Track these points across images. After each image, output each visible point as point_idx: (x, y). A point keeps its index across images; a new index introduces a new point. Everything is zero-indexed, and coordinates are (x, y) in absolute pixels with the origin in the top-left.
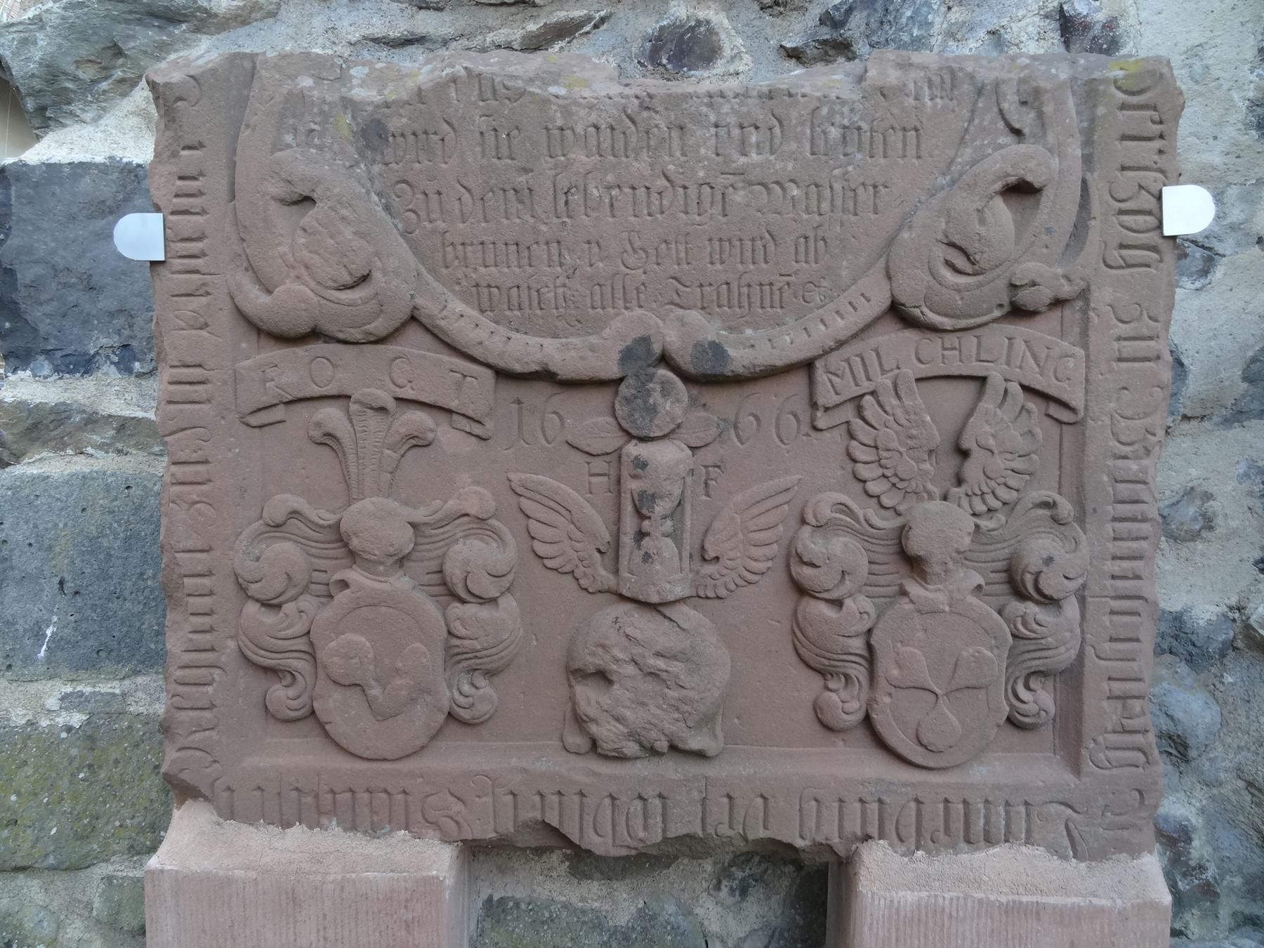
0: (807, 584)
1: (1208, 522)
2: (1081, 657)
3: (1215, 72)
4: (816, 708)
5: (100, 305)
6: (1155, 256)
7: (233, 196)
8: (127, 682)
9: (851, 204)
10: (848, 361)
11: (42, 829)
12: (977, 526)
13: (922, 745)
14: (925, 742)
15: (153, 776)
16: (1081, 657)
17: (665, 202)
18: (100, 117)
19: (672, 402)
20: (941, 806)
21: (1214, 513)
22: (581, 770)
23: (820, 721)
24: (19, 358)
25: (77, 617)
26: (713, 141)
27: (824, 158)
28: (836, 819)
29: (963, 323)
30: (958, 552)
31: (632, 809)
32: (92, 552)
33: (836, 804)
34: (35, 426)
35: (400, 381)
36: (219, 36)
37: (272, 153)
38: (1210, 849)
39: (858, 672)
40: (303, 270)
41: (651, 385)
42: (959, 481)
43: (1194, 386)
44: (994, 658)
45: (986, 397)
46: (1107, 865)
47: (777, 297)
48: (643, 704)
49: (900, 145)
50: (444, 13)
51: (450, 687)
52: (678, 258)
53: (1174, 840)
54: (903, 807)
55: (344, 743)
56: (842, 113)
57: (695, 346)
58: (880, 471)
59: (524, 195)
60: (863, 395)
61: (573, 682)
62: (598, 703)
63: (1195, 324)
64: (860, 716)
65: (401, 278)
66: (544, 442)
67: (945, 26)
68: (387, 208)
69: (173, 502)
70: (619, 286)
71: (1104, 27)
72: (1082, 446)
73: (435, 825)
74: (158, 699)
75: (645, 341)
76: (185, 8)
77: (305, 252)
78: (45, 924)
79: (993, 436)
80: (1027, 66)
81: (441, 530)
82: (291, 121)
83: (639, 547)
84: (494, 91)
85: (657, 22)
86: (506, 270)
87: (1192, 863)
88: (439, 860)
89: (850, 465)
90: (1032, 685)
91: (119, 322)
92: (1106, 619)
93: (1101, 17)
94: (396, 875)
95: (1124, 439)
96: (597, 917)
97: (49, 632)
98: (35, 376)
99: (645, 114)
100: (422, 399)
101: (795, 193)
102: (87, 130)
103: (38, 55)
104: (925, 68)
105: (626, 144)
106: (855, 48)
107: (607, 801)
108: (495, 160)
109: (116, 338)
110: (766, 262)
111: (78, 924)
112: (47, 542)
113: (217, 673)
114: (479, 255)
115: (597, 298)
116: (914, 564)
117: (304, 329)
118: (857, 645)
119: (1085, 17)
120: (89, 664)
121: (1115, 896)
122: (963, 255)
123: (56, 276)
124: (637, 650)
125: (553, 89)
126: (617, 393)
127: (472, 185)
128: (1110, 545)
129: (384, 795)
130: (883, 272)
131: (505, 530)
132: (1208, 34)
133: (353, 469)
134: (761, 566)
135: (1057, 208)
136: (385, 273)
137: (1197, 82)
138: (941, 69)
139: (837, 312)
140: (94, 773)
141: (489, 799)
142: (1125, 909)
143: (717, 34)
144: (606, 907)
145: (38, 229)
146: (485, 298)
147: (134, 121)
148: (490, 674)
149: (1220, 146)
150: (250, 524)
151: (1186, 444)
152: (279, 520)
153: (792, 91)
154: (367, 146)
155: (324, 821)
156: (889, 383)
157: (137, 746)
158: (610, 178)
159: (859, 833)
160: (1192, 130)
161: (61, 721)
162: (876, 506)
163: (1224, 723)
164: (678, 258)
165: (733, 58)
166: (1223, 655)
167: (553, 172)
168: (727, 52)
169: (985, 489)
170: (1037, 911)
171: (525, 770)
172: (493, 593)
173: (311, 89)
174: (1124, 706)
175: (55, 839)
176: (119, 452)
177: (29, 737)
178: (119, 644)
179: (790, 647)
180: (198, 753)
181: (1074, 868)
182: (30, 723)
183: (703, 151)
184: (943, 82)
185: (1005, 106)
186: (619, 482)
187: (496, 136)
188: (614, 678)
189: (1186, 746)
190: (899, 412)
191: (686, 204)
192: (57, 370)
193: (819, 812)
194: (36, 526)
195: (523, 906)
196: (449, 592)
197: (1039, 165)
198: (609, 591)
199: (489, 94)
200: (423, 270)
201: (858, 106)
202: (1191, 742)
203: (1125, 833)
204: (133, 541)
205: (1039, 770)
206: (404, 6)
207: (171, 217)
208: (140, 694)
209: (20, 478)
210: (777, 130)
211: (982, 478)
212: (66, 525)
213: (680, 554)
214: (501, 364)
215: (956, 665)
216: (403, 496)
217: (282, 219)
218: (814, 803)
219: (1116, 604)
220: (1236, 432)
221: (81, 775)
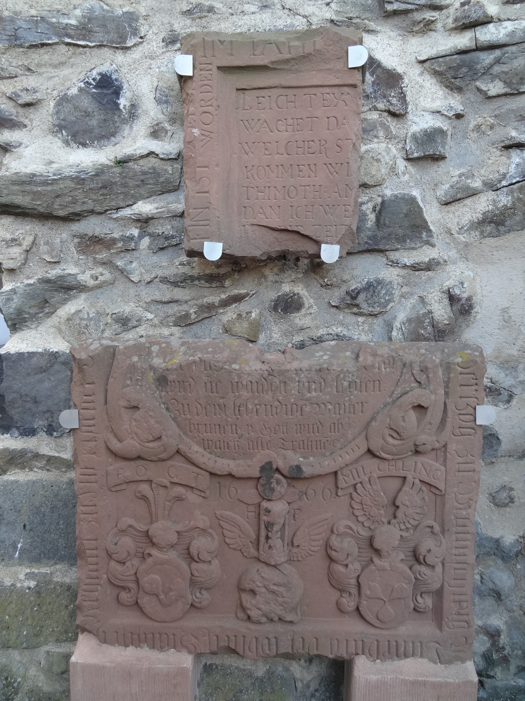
0: (334, 558)
1: (512, 500)
2: (442, 586)
3: (513, 319)
4: (337, 604)
5: (40, 409)
6: (474, 431)
7: (106, 403)
8: (52, 568)
9: (352, 410)
10: (351, 471)
11: (20, 631)
12: (401, 536)
13: (378, 619)
14: (380, 619)
15: (66, 610)
16: (442, 586)
17: (278, 411)
18: (38, 326)
19: (281, 487)
20: (387, 643)
21: (514, 496)
22: (243, 627)
23: (339, 609)
24: (6, 429)
25: (32, 540)
26: (297, 388)
27: (341, 394)
28: (345, 647)
29: (396, 457)
30: (393, 547)
31: (264, 642)
32: (37, 513)
33: (345, 642)
34: (12, 458)
35: (172, 476)
36: (89, 294)
37: (122, 389)
38: (508, 639)
39: (354, 591)
40: (134, 435)
41: (272, 480)
42: (395, 517)
44: (408, 588)
45: (405, 485)
46: (452, 666)
47: (322, 445)
48: (269, 603)
49: (372, 387)
50: (186, 289)
51: (192, 594)
52: (283, 432)
54: (371, 643)
55: (150, 615)
56: (349, 377)
57: (290, 467)
58: (363, 513)
59: (223, 407)
60: (357, 484)
61: (240, 592)
62: (250, 602)
63: (504, 423)
64: (355, 607)
65: (173, 436)
66: (229, 499)
67: (400, 293)
68: (167, 409)
69: (82, 521)
70: (259, 442)
71: (466, 300)
72: (443, 504)
73: (186, 647)
74: (66, 575)
75: (270, 463)
76: (75, 285)
77: (135, 429)
78: (21, 669)
79: (409, 501)
80: (423, 355)
81: (188, 533)
82: (129, 375)
83: (267, 542)
84: (210, 367)
85: (277, 294)
86: (215, 434)
87: (500, 646)
88: (186, 660)
89: (351, 510)
90: (423, 596)
91: (48, 415)
92: (452, 572)
93: (465, 295)
94: (170, 666)
95: (460, 502)
96: (250, 672)
97: (19, 546)
98: (11, 437)
99: (270, 377)
100: (180, 483)
101: (330, 407)
102: (34, 332)
103: (14, 306)
104: (382, 356)
105: (263, 388)
106: (361, 305)
107: (254, 639)
108: (210, 393)
109: (46, 422)
110: (318, 433)
111: (34, 668)
112: (18, 509)
113: (99, 587)
114: (204, 428)
115: (251, 446)
117: (135, 456)
118: (353, 581)
119: (459, 295)
120: (36, 560)
121: (454, 678)
122: (397, 433)
123: (21, 397)
124: (266, 583)
125: (234, 366)
126: (258, 482)
127: (201, 402)
128: (454, 543)
129: (166, 636)
130: (365, 437)
131: (214, 534)
132: (511, 303)
133: (153, 509)
134: (316, 549)
135: (434, 415)
136: (167, 436)
137: (506, 322)
138: (389, 357)
139: (347, 452)
140: (40, 608)
141: (207, 638)
142: (459, 683)
143: (302, 298)
144: (253, 668)
145: (14, 379)
147: (53, 330)
148: (207, 589)
149: (516, 347)
150: (112, 529)
151: (503, 466)
152: (124, 529)
153: (329, 368)
154: (159, 385)
155: (142, 645)
156: (367, 479)
157: (58, 596)
158: (256, 401)
159: (354, 652)
160: (505, 340)
161: (26, 584)
162: (362, 526)
163: (516, 585)
164: (283, 432)
165: (309, 308)
166: (517, 556)
167: (234, 399)
168: (306, 305)
169: (405, 520)
170: (424, 684)
171: (222, 627)
172: (209, 559)
173: (137, 362)
174: (460, 604)
175: (26, 636)
176: (48, 470)
177: (13, 591)
178: (49, 551)
179: (327, 580)
180: (91, 618)
181: (439, 667)
182: (13, 585)
183: (293, 392)
184: (389, 362)
185: (414, 372)
186: (259, 514)
187: (211, 384)
188: (257, 593)
189: (500, 595)
190: (371, 491)
191: (286, 412)
192: (21, 434)
193: (338, 644)
194: (13, 502)
195: (219, 668)
196: (190, 557)
197: (426, 399)
198: (255, 557)
199: (208, 368)
200: (182, 434)
201: (355, 374)
202: (502, 593)
203: (460, 654)
204: (54, 509)
205: (426, 629)
206: (169, 286)
207: (81, 411)
208: (58, 573)
209: (7, 481)
210: (323, 383)
211: (404, 516)
212: (26, 502)
213: (283, 545)
214: (212, 471)
215: (392, 590)
216: (173, 519)
217: (126, 415)
218: (336, 641)
219: (456, 566)
221: (35, 609)
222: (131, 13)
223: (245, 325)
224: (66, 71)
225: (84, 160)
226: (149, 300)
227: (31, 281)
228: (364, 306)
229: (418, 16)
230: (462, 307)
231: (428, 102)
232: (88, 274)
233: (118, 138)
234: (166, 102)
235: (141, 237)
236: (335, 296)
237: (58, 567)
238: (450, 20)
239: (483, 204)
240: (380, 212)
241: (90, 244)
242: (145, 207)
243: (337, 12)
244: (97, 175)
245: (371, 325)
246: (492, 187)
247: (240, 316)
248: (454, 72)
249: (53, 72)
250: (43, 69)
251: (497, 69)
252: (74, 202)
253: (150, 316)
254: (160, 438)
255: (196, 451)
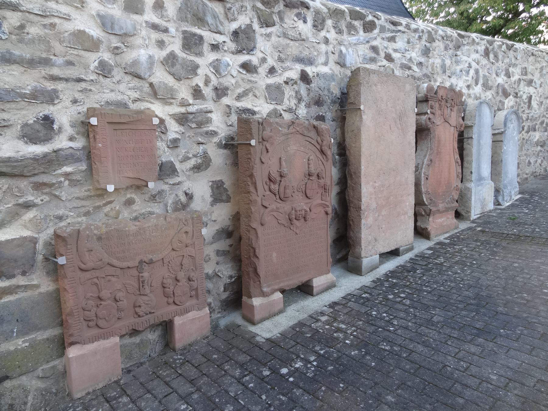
1: (210, 259)
19: (146, 267)
22: (138, 320)
39: (172, 296)
43: (206, 241)
53: (209, 305)
88: (117, 339)
116: (178, 281)
118: (172, 293)
120: (27, 334)
122: (181, 242)
135: (190, 234)
146: (118, 259)
147: (20, 226)
161: (24, 345)
196: (116, 300)
205: (194, 301)
217: (87, 254)
220: (212, 245)
222: (55, 89)
223: (114, 212)
224: (24, 112)
225: (36, 150)
226: (71, 207)
227: (10, 206)
228: (158, 200)
229: (168, 101)
230: (189, 196)
231: (174, 129)
232: (39, 199)
233: (53, 141)
234: (75, 127)
235: (65, 181)
236: (147, 197)
237: (38, 333)
238: (178, 103)
239: (192, 162)
240: (161, 166)
241: (38, 187)
242: (68, 169)
243: (139, 95)
244: (44, 157)
245: (159, 206)
246: (195, 156)
247: (112, 209)
248: (182, 119)
249: (16, 112)
250: (11, 110)
251: (194, 120)
252: (34, 169)
253: (72, 214)
254: (101, 260)
255: (115, 262)
